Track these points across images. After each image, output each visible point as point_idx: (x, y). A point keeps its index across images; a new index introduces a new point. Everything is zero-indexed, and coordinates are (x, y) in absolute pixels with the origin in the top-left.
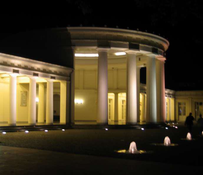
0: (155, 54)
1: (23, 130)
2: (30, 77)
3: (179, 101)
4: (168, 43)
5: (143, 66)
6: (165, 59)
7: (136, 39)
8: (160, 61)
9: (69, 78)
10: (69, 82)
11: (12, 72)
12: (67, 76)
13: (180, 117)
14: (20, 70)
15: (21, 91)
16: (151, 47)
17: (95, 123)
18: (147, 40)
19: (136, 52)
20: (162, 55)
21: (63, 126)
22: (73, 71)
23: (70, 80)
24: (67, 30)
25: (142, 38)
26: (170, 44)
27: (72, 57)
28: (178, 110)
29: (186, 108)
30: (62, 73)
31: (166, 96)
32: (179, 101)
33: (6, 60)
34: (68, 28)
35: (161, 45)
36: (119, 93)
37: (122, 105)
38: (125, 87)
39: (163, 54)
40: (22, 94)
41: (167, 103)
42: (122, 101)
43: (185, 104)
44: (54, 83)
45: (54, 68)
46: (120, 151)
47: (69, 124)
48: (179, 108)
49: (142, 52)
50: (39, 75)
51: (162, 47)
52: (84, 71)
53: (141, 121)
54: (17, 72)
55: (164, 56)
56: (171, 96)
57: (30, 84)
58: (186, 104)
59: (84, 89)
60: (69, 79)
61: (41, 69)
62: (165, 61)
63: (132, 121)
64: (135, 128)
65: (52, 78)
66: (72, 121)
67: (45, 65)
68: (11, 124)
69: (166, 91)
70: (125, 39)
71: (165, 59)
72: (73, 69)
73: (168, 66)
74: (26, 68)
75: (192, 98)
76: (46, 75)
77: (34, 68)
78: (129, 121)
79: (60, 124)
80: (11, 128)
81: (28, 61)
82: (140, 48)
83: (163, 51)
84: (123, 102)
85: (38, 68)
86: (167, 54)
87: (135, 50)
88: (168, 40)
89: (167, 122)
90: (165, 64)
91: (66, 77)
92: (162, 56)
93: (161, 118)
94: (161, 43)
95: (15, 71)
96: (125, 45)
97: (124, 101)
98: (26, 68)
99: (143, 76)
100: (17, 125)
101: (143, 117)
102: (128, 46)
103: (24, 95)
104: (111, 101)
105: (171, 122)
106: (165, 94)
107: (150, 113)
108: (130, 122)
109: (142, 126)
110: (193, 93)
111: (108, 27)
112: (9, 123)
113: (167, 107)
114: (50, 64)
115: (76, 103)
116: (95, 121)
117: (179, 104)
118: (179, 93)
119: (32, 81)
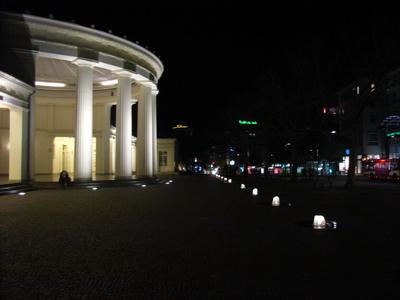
4: (159, 69)
10: (27, 110)
12: (23, 99)
16: (149, 72)
19: (93, 64)
21: (17, 186)
23: (29, 107)
24: (23, 19)
27: (31, 61)
34: (25, 16)
46: (62, 85)
47: (27, 183)
49: (101, 65)
52: (54, 106)
60: (26, 103)
64: (132, 185)
66: (32, 177)
70: (119, 54)
73: (160, 100)
91: (13, 98)
96: (72, 49)
111: (96, 28)
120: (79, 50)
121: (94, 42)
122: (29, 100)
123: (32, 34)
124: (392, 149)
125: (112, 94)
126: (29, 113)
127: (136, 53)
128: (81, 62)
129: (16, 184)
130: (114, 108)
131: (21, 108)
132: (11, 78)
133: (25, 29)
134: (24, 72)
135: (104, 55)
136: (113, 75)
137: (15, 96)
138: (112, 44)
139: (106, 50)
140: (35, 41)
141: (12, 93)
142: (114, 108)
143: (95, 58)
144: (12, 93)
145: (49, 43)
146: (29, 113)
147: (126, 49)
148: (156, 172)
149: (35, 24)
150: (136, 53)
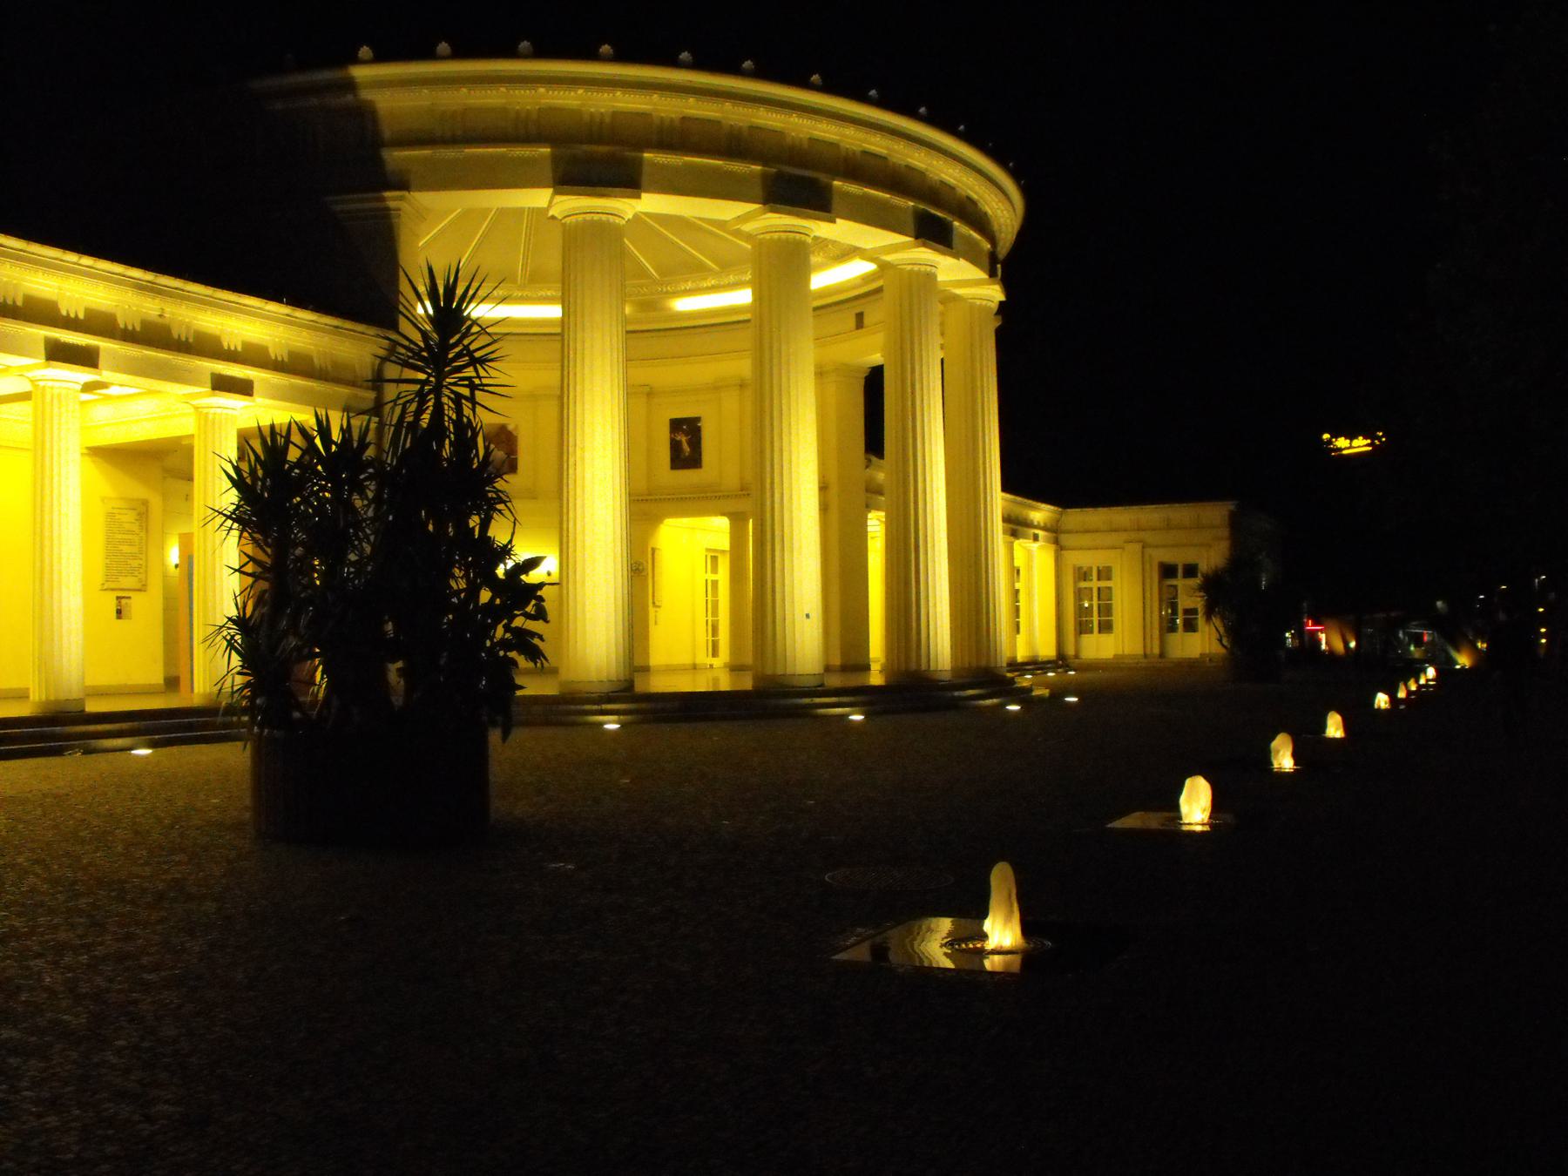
0: (943, 253)
1: (119, 742)
2: (196, 402)
3: (1076, 558)
4: (1004, 208)
7: (806, 146)
8: (971, 307)
9: (371, 395)
11: (41, 360)
12: (352, 383)
13: (1086, 638)
14: (104, 345)
15: (103, 500)
19: (626, 208)
20: (982, 269)
24: (350, 86)
28: (1083, 610)
30: (311, 359)
32: (1076, 558)
35: (974, 203)
37: (711, 577)
39: (986, 261)
40: (110, 516)
43: (1104, 574)
48: (1079, 594)
49: (651, 203)
51: (980, 222)
53: (875, 667)
54: (86, 358)
55: (992, 274)
56: (1041, 533)
57: (196, 443)
58: (1116, 573)
64: (955, 705)
65: (222, 384)
68: (48, 702)
70: (735, 145)
74: (153, 336)
80: (55, 730)
81: (140, 287)
82: (836, 203)
84: (714, 559)
85: (248, 346)
86: (1009, 268)
87: (798, 215)
88: (1015, 175)
89: (1014, 666)
90: (1005, 340)
91: (344, 391)
92: (984, 276)
94: (975, 197)
98: (153, 336)
99: (873, 413)
100: (92, 707)
102: (758, 191)
103: (129, 518)
105: (1035, 665)
107: (978, 628)
108: (924, 667)
110: (1150, 514)
117: (1083, 575)
118: (1077, 517)
119: (206, 421)
120: (555, 159)
123: (387, 134)
125: (860, 318)
129: (1049, 662)
130: (874, 381)
132: (273, 307)
133: (364, 116)
135: (853, 188)
136: (701, 247)
137: (337, 380)
138: (877, 144)
142: (874, 381)
143: (628, 180)
145: (449, 153)
147: (919, 160)
148: (805, 641)
149: (392, 88)
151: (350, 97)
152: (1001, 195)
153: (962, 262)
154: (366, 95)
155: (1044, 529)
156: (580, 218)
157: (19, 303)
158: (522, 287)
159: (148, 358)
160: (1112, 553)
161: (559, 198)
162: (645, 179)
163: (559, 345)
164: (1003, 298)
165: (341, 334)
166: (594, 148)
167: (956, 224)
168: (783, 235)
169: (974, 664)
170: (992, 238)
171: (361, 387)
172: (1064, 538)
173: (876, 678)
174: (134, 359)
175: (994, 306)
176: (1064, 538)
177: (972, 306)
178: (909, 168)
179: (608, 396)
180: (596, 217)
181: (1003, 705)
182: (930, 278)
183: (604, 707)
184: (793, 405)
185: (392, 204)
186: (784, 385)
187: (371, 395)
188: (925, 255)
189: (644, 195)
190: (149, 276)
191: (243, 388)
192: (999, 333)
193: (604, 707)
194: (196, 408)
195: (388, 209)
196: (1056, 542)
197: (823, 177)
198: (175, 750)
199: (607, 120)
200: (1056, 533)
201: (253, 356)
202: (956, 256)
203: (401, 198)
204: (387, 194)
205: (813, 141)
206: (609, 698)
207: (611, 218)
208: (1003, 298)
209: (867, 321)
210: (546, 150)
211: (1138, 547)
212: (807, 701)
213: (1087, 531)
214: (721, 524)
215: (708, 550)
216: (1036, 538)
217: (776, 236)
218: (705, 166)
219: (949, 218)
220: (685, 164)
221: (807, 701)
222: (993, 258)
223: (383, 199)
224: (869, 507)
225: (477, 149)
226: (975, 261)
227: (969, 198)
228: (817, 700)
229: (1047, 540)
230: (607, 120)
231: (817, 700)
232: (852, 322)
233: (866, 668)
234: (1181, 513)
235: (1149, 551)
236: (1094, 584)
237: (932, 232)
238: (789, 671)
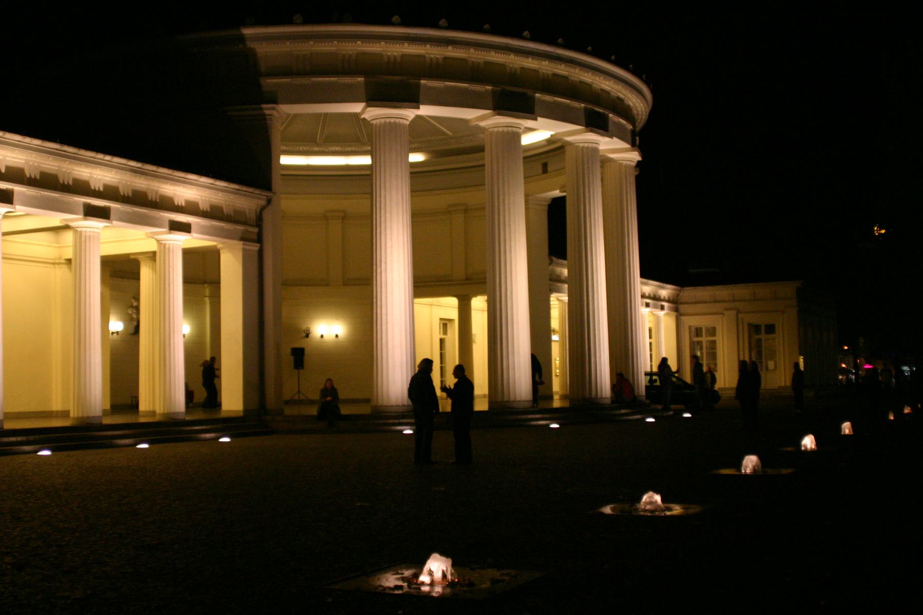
0: (602, 135)
1: (127, 441)
5: (557, 193)
6: (635, 156)
9: (256, 230)
10: (255, 247)
11: (81, 216)
12: (244, 223)
14: (18, 189)
17: (365, 410)
18: (566, 78)
20: (626, 142)
21: (230, 425)
22: (269, 201)
23: (259, 239)
24: (242, 39)
25: (545, 67)
26: (652, 91)
29: (719, 346)
30: (222, 208)
31: (647, 305)
33: (142, 183)
34: (247, 31)
36: (475, 295)
37: (443, 337)
38: (482, 270)
39: (629, 137)
41: (650, 330)
42: (438, 321)
44: (189, 255)
45: (189, 189)
47: (256, 419)
49: (426, 110)
50: (16, 198)
52: (344, 217)
53: (556, 397)
54: (102, 214)
55: (633, 144)
56: (666, 304)
58: (719, 332)
59: (346, 283)
60: (252, 230)
61: (203, 206)
62: (639, 163)
63: (380, 403)
65: (176, 227)
67: (236, 192)
69: (641, 287)
70: (476, 74)
71: (635, 156)
72: (269, 194)
74: (138, 199)
75: (738, 312)
76: (56, 200)
77: (173, 202)
78: (499, 399)
79: (223, 415)
81: (134, 171)
83: (630, 127)
84: (445, 326)
85: (106, 187)
86: (640, 139)
88: (647, 82)
91: (240, 228)
92: (627, 146)
93: (165, 388)
94: (622, 96)
95: (91, 212)
97: (451, 320)
98: (138, 199)
99: (557, 235)
101: (563, 386)
104: (448, 326)
106: (643, 296)
109: (555, 414)
110: (741, 291)
112: (72, 415)
113: (651, 344)
114: (71, 150)
115: (319, 335)
116: (367, 401)
117: (698, 332)
118: (690, 293)
120: (366, 84)
121: (487, 63)
122: (259, 221)
123: (263, 69)
124: (671, 305)
126: (261, 253)
127: (530, 63)
128: (374, 114)
131: (239, 245)
133: (250, 57)
134: (241, 159)
135: (548, 98)
138: (451, 52)
139: (554, 85)
140: (270, 83)
141: (213, 213)
142: (557, 209)
143: (414, 100)
144: (213, 213)
146: (261, 253)
149: (267, 42)
150: (530, 63)
151: (241, 46)
152: (640, 97)
153: (615, 139)
154: (250, 44)
155: (668, 301)
156: (383, 121)
157: (71, 183)
158: (318, 145)
159: (135, 213)
160: (714, 317)
161: (369, 109)
162: (421, 97)
163: (369, 201)
164: (639, 158)
165: (241, 195)
166: (390, 78)
167: (611, 115)
168: (505, 129)
169: (80, 415)
170: (634, 126)
171: (250, 225)
172: (683, 308)
173: (557, 403)
174: (128, 213)
175: (634, 164)
176: (683, 308)
177: (621, 164)
178: (581, 82)
179: (401, 232)
180: (392, 120)
181: (644, 419)
182: (596, 150)
183: (401, 421)
184: (512, 235)
185: (267, 112)
186: (507, 222)
187: (256, 230)
188: (591, 137)
189: (421, 107)
190: (139, 165)
191: (185, 228)
192: (637, 177)
193: (401, 421)
194: (158, 241)
195: (265, 115)
196: (676, 310)
197: (529, 92)
198: (161, 445)
199: (399, 59)
200: (676, 304)
201: (191, 209)
202: (611, 137)
203: (273, 109)
204: (264, 106)
205: (523, 68)
206: (404, 417)
207: (401, 121)
208: (639, 158)
209: (550, 168)
210: (361, 79)
211: (734, 312)
212: (523, 417)
213: (696, 303)
214: (453, 301)
215: (441, 319)
216: (662, 308)
217: (501, 129)
218: (456, 87)
219: (606, 112)
220: (446, 86)
221: (523, 417)
222: (633, 133)
223: (261, 109)
224: (552, 291)
225: (322, 77)
226: (622, 139)
227: (618, 98)
228: (530, 416)
229: (671, 309)
230: (399, 59)
231: (530, 416)
232: (540, 170)
233: (550, 397)
234: (763, 290)
235: (740, 316)
236: (704, 339)
237: (596, 123)
238: (512, 399)
